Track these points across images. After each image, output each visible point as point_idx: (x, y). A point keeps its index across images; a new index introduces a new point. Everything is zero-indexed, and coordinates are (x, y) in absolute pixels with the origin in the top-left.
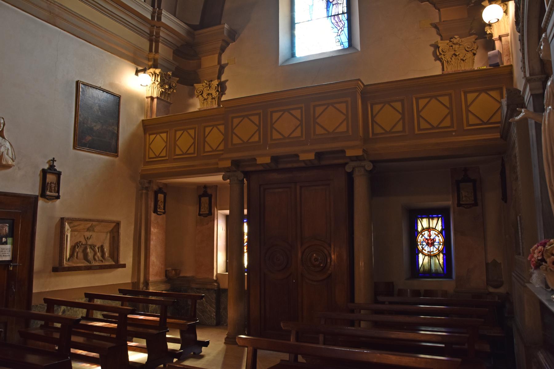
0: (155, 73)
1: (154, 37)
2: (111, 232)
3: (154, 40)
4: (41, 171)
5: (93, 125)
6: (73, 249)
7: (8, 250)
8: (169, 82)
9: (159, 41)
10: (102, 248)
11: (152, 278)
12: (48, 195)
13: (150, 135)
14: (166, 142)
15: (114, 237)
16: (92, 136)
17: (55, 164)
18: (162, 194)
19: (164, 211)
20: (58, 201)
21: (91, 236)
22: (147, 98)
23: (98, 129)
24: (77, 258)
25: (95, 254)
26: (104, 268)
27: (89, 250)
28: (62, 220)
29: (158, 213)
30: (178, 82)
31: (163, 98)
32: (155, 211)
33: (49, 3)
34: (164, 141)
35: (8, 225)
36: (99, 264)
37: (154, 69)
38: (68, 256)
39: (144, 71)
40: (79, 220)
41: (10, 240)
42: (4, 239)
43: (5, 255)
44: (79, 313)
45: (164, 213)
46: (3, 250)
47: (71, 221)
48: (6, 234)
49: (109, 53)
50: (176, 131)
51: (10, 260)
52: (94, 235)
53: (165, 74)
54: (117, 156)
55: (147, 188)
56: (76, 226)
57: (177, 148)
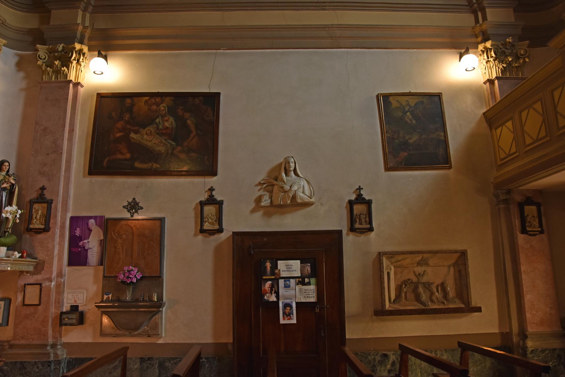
0: (486, 48)
1: (476, 5)
2: (455, 264)
3: (477, 9)
4: (348, 203)
5: (407, 138)
6: (399, 289)
7: (312, 291)
8: (514, 51)
9: (485, 7)
10: (443, 286)
11: (530, 329)
12: (358, 227)
13: (496, 129)
14: (514, 133)
15: (460, 271)
16: (407, 151)
17: (362, 192)
18: (534, 205)
19: (539, 229)
20: (373, 234)
21: (425, 271)
22: (485, 83)
23: (415, 142)
24: (406, 298)
25: (432, 294)
26: (444, 313)
27: (421, 290)
28: (380, 255)
29: (529, 233)
30: (530, 46)
31: (508, 76)
32: (524, 231)
33: (328, 29)
34: (511, 131)
35: (309, 264)
36: (438, 307)
37: (483, 44)
38: (393, 297)
39: (467, 52)
40: (402, 253)
41: (313, 280)
42: (306, 279)
43: (309, 296)
44: (415, 368)
45: (542, 232)
46: (307, 291)
47: (391, 255)
48: (308, 274)
49: (415, 50)
50: (521, 112)
51: (315, 301)
52: (429, 270)
53: (502, 44)
54: (450, 168)
55: (506, 201)
56: (400, 261)
57: (526, 136)
